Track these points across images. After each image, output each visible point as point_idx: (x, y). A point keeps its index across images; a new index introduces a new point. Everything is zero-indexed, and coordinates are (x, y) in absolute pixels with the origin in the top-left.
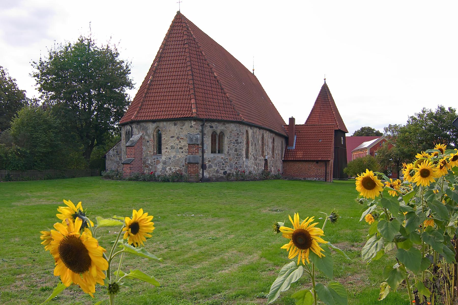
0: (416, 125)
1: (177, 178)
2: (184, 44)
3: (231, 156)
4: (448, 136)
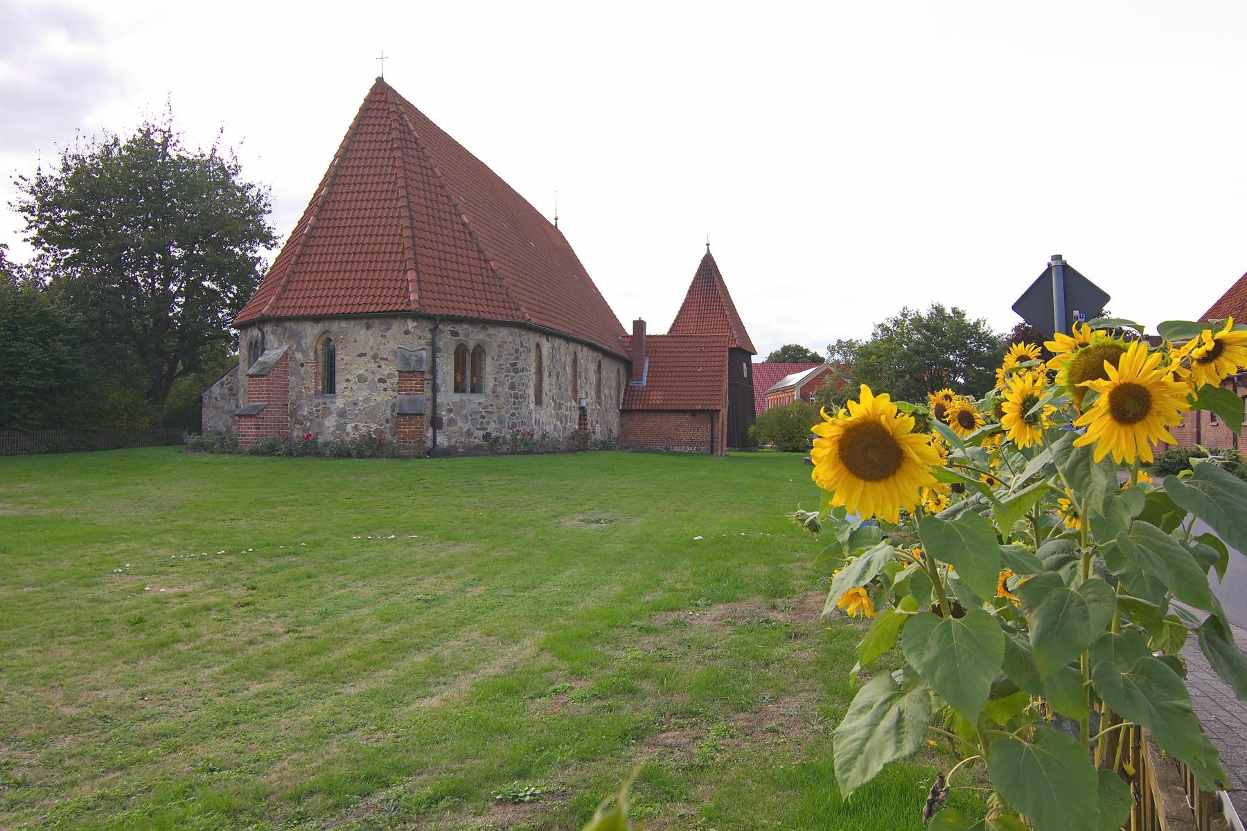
0: (890, 340)
1: (371, 449)
2: (392, 150)
3: (502, 400)
4: (951, 364)
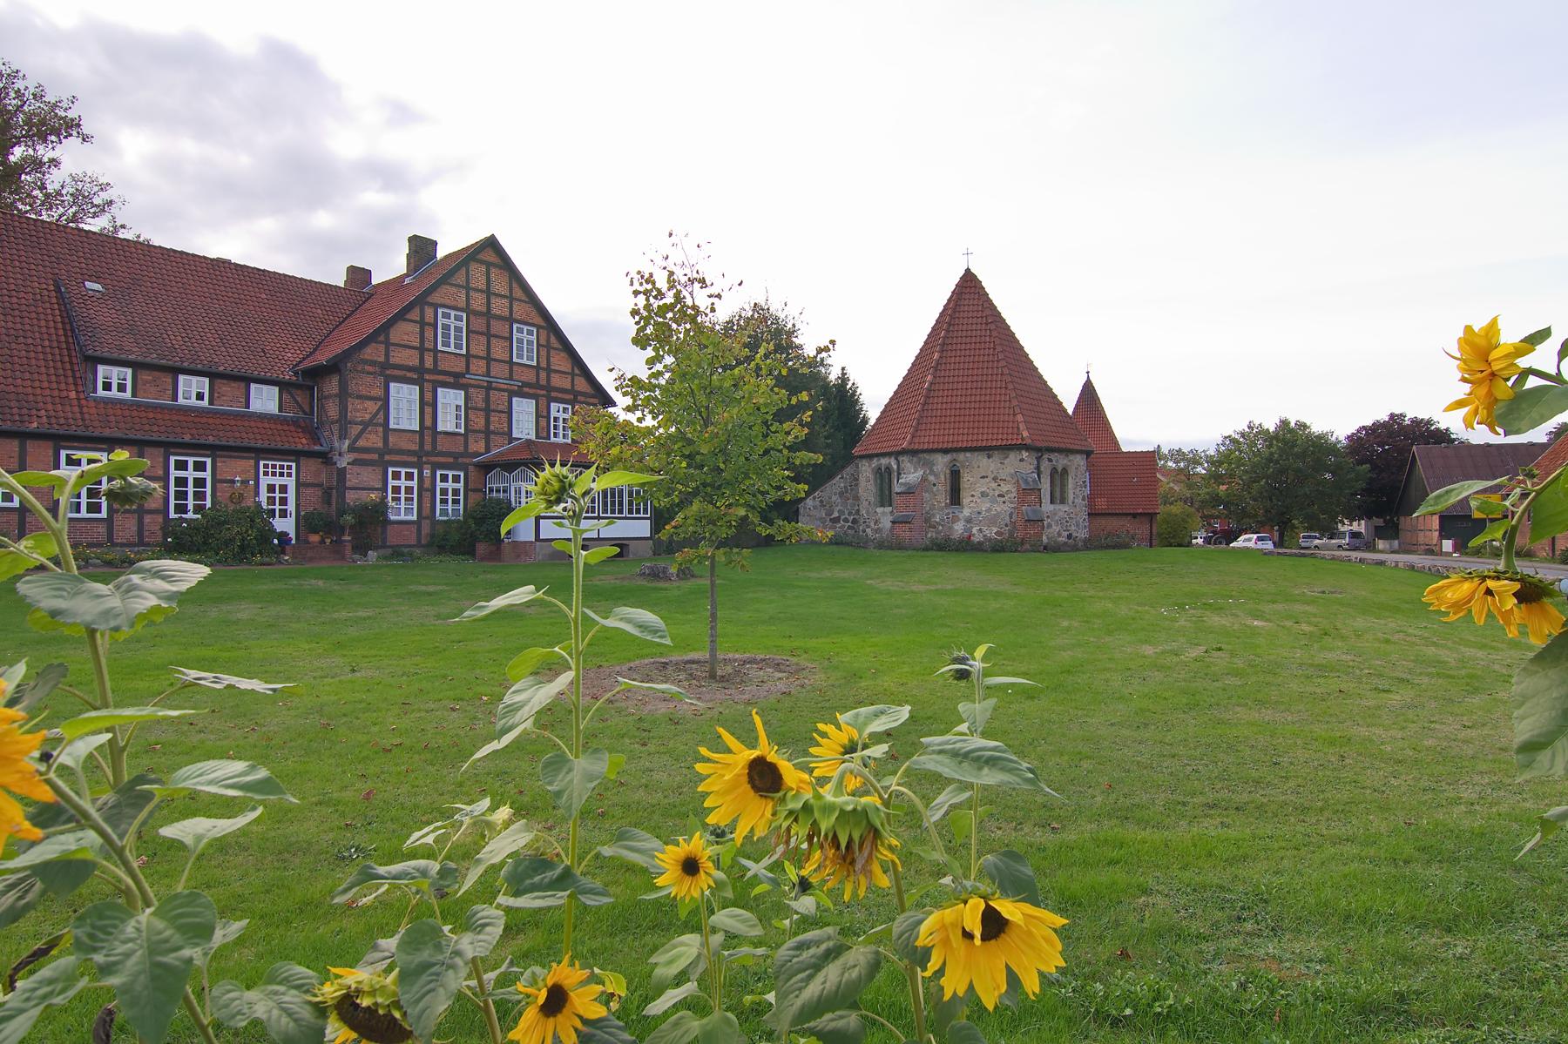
1: (998, 547)
